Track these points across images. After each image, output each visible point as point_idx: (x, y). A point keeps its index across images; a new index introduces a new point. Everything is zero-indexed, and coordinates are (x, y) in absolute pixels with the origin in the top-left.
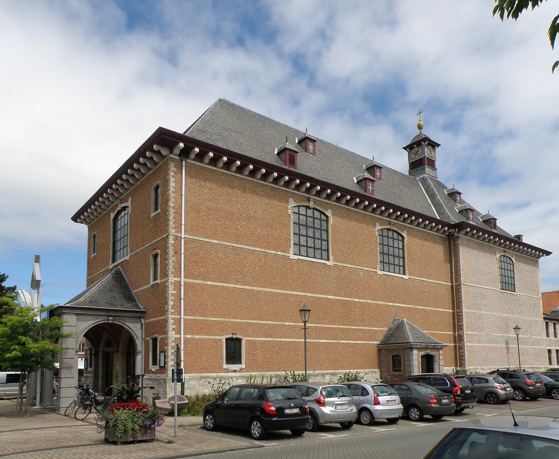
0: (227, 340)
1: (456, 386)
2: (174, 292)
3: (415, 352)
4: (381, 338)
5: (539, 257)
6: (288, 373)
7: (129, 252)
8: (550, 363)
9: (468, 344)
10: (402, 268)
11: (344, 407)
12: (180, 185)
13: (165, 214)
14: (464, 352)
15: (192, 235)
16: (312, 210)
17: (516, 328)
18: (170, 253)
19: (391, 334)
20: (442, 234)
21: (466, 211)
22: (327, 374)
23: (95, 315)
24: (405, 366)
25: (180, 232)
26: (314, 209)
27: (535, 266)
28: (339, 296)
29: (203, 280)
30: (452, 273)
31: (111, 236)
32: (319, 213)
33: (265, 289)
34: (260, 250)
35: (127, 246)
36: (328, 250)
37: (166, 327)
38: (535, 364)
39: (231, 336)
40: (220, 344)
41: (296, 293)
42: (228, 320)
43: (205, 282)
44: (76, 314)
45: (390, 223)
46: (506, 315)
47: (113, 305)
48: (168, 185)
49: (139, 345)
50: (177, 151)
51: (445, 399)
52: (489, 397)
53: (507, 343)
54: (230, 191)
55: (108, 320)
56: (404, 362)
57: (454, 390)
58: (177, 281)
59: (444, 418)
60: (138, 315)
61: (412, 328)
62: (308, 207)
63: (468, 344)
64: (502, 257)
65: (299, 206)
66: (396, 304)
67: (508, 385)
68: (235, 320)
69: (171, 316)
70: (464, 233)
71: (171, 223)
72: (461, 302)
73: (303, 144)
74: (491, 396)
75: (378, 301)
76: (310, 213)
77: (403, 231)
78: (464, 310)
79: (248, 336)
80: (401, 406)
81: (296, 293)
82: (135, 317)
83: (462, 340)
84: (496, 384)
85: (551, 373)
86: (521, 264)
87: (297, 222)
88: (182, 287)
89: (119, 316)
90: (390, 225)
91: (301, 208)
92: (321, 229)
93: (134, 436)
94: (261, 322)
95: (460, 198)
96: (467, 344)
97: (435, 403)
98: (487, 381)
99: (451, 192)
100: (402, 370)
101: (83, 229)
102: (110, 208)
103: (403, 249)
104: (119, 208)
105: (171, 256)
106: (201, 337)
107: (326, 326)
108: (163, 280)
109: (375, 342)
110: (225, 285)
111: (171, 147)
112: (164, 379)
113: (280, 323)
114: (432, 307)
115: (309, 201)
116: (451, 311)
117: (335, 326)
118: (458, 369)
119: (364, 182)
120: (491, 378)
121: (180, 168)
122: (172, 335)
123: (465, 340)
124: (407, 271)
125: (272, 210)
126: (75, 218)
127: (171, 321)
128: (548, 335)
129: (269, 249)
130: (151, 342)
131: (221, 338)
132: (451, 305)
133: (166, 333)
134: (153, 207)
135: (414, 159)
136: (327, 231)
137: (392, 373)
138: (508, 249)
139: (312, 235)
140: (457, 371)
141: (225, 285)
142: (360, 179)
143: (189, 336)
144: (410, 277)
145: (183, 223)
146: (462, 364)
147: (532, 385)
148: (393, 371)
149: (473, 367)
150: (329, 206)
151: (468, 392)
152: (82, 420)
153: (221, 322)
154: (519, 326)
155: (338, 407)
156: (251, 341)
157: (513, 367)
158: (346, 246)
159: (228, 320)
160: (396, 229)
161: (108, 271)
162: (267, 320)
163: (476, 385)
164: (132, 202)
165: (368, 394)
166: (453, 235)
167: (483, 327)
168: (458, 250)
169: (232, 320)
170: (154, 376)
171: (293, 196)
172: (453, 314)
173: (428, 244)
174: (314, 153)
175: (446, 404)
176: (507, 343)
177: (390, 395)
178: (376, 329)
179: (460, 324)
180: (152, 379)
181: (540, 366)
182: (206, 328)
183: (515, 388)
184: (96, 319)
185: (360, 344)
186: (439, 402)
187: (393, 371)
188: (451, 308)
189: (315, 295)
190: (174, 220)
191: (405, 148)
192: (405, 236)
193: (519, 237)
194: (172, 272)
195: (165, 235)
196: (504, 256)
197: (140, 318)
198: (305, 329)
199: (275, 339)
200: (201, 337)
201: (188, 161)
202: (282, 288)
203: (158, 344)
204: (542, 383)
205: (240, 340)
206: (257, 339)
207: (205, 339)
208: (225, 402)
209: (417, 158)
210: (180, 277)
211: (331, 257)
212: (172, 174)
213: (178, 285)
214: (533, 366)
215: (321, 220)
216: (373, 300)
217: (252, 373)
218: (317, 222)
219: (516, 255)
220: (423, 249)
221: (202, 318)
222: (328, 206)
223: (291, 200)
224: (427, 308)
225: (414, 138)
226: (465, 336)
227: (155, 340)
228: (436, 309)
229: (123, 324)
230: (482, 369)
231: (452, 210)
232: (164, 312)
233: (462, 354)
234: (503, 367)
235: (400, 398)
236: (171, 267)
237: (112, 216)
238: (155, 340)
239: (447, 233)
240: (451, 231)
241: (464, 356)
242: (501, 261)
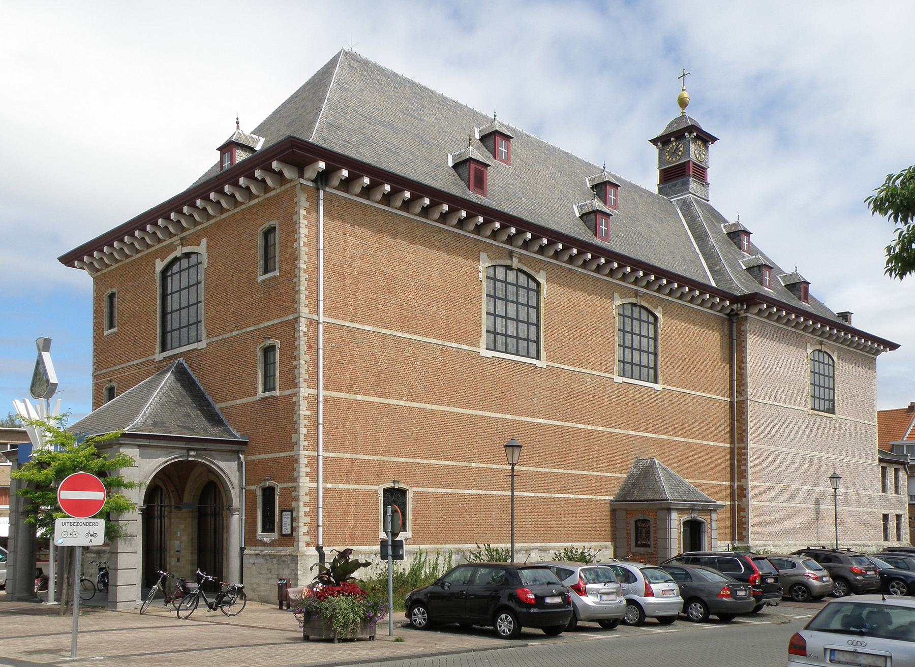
0: (385, 491)
1: (754, 572)
2: (308, 413)
3: (674, 515)
4: (617, 490)
5: (878, 352)
6: (482, 546)
7: (204, 335)
8: (886, 538)
9: (754, 503)
10: (652, 371)
11: (612, 597)
12: (319, 236)
13: (290, 280)
14: (746, 517)
15: (334, 317)
16: (515, 272)
17: (834, 477)
18: (301, 348)
19: (633, 484)
20: (720, 311)
21: (758, 269)
22: (533, 549)
23: (161, 447)
24: (656, 539)
25: (316, 313)
26: (519, 270)
27: (869, 369)
28: (554, 419)
29: (350, 392)
30: (731, 380)
31: (158, 302)
32: (526, 278)
33: (442, 408)
34: (435, 341)
35: (198, 322)
36: (538, 342)
37: (294, 470)
38: (863, 536)
39: (391, 485)
40: (374, 498)
41: (488, 414)
42: (387, 458)
43: (352, 396)
44: (139, 446)
45: (636, 294)
46: (817, 454)
47: (192, 430)
48: (296, 232)
49: (237, 498)
50: (311, 173)
51: (741, 590)
52: (795, 591)
53: (817, 502)
54: (391, 241)
55: (188, 456)
56: (656, 532)
57: (751, 579)
58: (311, 394)
59: (735, 619)
60: (236, 447)
61: (669, 476)
62: (509, 268)
63: (754, 503)
64: (816, 352)
65: (494, 266)
66: (641, 434)
67: (825, 572)
68: (398, 459)
69: (303, 453)
70: (756, 311)
71: (303, 297)
72: (745, 431)
73: (490, 143)
74: (800, 588)
75: (613, 427)
76: (511, 277)
77: (656, 308)
78: (751, 445)
79: (416, 485)
80: (680, 599)
81: (488, 414)
82: (230, 451)
83: (745, 496)
84: (808, 571)
85: (889, 554)
86: (846, 365)
87: (492, 294)
88: (321, 405)
89: (205, 450)
90: (636, 296)
91: (498, 269)
92: (528, 306)
93: (353, 631)
94: (436, 462)
95: (748, 241)
96: (753, 503)
97: (727, 596)
98: (794, 565)
99: (733, 229)
100: (652, 545)
101: (82, 280)
102: (150, 250)
103: (655, 339)
104: (178, 253)
105: (302, 352)
106: (347, 486)
107: (532, 469)
108: (287, 392)
109: (607, 498)
110: (383, 400)
111: (301, 167)
112: (291, 555)
113: (464, 464)
114: (698, 438)
115: (511, 257)
116: (728, 445)
117: (547, 470)
118: (737, 544)
119: (592, 216)
120: (799, 561)
121: (315, 202)
122: (305, 483)
123: (750, 496)
124: (660, 377)
125: (454, 273)
126: (68, 260)
127: (303, 461)
128: (884, 491)
129: (449, 341)
130: (259, 493)
131: (376, 488)
132: (728, 436)
133: (296, 480)
134: (260, 264)
135: (669, 163)
136: (537, 308)
137: (634, 549)
138: (827, 338)
139: (513, 316)
140: (734, 548)
141: (383, 400)
142: (586, 210)
143: (329, 486)
144: (665, 386)
145: (321, 298)
146: (743, 537)
147: (861, 574)
148: (637, 545)
149: (761, 542)
150: (542, 265)
151: (770, 581)
152: (186, 618)
153: (377, 463)
154: (838, 473)
155: (605, 597)
156: (421, 493)
157: (827, 542)
158: (566, 334)
159: (387, 458)
160: (646, 305)
161: (160, 368)
162: (445, 460)
163: (782, 571)
164: (208, 247)
165: (636, 580)
166: (737, 314)
167: (779, 474)
168: (745, 341)
169: (393, 459)
170: (268, 551)
171: (487, 248)
172: (732, 450)
173: (696, 329)
174: (507, 160)
175: (742, 598)
176: (817, 502)
177: (666, 581)
178: (609, 475)
179: (743, 468)
180: (264, 555)
181: (869, 543)
182: (352, 472)
183: (836, 577)
184: (170, 453)
185: (584, 500)
186: (733, 594)
187: (637, 545)
188: (728, 440)
189: (517, 418)
190: (306, 292)
191: (654, 142)
192: (659, 315)
193: (845, 316)
194: (305, 380)
195: (291, 317)
196: (820, 351)
197: (237, 452)
198: (513, 476)
199: (457, 491)
200: (347, 486)
201: (327, 189)
202: (468, 405)
203: (277, 498)
204: (875, 571)
205: (403, 492)
206: (431, 490)
207: (354, 490)
208: (446, 588)
209: (676, 161)
210: (317, 388)
211: (543, 354)
212: (303, 212)
213: (314, 402)
214: (857, 542)
215: (528, 289)
216: (605, 426)
217: (422, 547)
218: (522, 292)
219: (839, 349)
220: (688, 339)
221: (348, 456)
222: (545, 266)
223: (483, 255)
224: (691, 440)
225: (671, 125)
226: (750, 490)
227: (269, 493)
228: (705, 442)
229: (211, 462)
230: (775, 546)
231: (734, 266)
232: (292, 445)
233: (744, 520)
234: (815, 543)
235: (680, 587)
236: (303, 371)
237: (160, 265)
238: (269, 493)
239: (728, 311)
240: (735, 307)
241: (746, 523)
242: (814, 360)
